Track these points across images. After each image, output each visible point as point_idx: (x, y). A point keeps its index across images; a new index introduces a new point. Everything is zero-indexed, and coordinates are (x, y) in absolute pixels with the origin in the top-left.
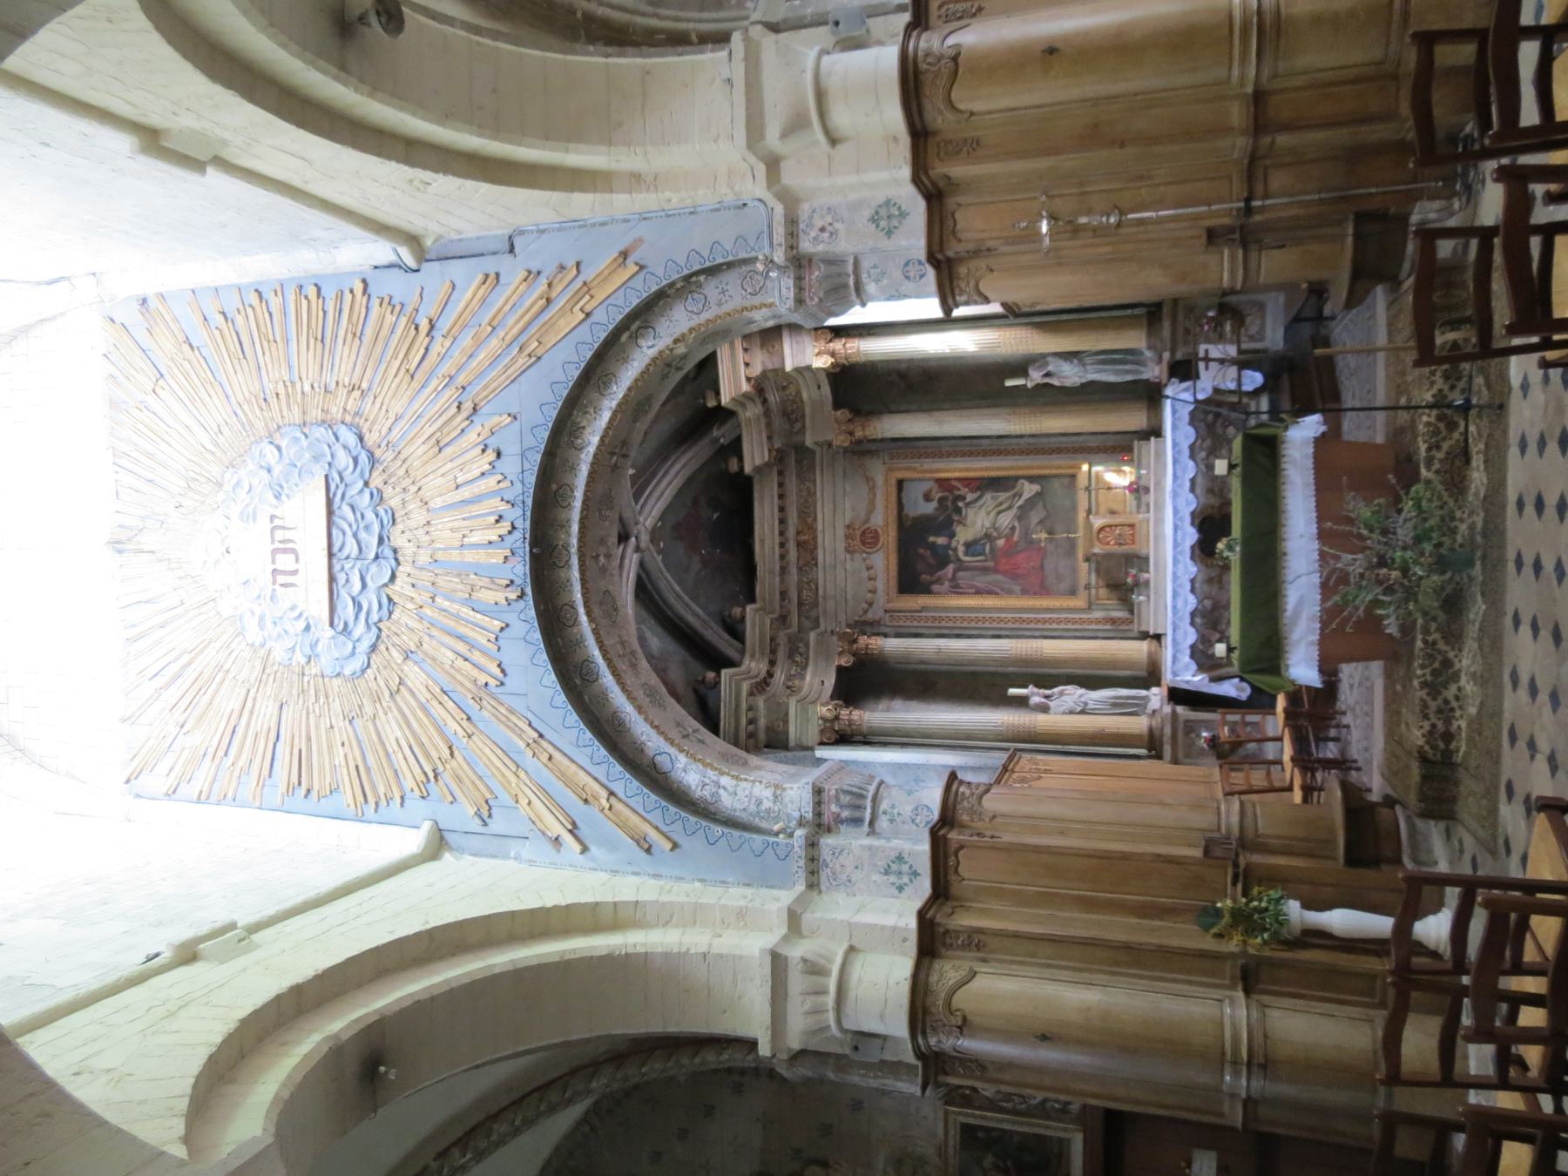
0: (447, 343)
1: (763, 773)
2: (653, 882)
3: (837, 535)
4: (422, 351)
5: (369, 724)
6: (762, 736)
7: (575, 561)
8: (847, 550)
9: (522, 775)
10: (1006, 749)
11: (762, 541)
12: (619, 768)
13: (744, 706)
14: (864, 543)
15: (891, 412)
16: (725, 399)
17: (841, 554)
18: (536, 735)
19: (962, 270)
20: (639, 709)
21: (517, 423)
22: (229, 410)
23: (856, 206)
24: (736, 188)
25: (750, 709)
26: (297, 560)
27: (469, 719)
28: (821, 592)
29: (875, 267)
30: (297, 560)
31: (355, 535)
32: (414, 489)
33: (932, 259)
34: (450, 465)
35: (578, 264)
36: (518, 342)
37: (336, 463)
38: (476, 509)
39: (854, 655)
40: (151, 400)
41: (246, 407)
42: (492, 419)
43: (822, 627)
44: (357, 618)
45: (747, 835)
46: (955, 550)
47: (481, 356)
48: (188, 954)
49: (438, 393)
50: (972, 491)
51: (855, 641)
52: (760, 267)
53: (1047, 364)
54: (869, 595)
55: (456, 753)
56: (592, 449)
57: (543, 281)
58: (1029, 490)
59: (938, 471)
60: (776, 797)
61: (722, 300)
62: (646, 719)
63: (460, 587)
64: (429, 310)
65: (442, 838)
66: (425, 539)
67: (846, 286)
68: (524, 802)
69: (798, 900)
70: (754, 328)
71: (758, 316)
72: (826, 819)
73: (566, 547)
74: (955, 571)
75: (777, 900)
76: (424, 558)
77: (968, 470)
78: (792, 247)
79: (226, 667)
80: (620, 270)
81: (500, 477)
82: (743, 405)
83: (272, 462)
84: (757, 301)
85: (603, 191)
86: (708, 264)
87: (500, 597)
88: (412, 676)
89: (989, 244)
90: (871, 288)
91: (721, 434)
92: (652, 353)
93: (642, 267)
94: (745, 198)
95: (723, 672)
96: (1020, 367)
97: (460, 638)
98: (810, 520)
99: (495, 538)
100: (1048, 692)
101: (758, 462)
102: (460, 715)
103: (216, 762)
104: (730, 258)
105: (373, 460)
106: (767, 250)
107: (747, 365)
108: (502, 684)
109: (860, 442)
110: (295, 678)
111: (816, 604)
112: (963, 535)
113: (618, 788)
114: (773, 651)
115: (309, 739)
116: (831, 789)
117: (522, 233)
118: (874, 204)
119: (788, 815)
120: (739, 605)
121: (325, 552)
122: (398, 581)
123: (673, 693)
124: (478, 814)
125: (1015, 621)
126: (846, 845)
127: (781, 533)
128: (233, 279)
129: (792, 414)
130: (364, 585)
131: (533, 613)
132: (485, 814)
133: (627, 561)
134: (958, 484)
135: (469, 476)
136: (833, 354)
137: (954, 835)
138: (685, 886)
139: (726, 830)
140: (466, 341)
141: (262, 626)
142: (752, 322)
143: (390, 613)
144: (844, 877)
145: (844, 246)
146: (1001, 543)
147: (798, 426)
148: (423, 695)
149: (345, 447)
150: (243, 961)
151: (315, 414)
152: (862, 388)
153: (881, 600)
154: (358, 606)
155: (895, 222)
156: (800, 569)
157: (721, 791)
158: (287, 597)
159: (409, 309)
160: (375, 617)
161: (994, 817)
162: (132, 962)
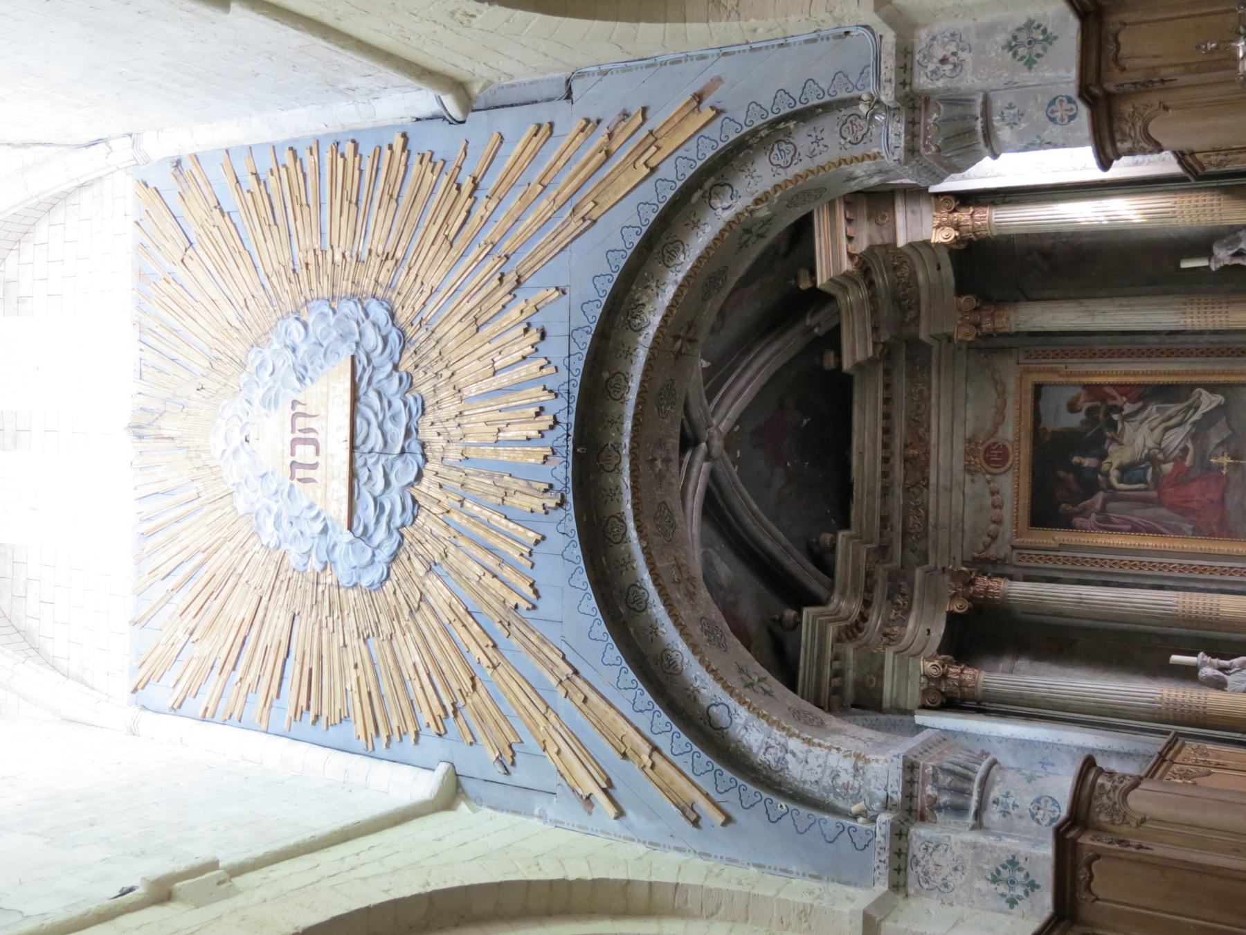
0: (492, 206)
1: (842, 738)
2: (698, 862)
3: (957, 452)
4: (464, 214)
5: (386, 644)
6: (850, 693)
7: (626, 465)
8: (967, 469)
9: (552, 718)
10: (1167, 733)
11: (861, 454)
12: (665, 718)
13: (829, 654)
14: (988, 461)
15: (1029, 299)
16: (822, 280)
17: (959, 475)
18: (570, 671)
19: (1127, 109)
20: (694, 648)
21: (566, 298)
22: (257, 282)
23: (988, 31)
24: (837, 13)
25: (836, 658)
26: (317, 453)
27: (495, 646)
28: (931, 520)
29: (1011, 107)
30: (317, 453)
31: (381, 426)
32: (446, 373)
33: (1085, 93)
34: (488, 347)
35: (644, 110)
36: (572, 204)
37: (364, 342)
38: (515, 399)
39: (970, 599)
40: (179, 271)
41: (274, 279)
42: (534, 294)
43: (932, 563)
44: (378, 521)
45: (817, 815)
46: (1107, 475)
47: (529, 221)
48: (162, 893)
49: (479, 263)
50: (1132, 401)
51: (972, 582)
52: (863, 109)
53: (1239, 240)
54: (993, 526)
55: (479, 686)
56: (651, 331)
57: (603, 130)
58: (1208, 401)
59: (1087, 374)
60: (856, 769)
61: (819, 148)
62: (701, 661)
63: (493, 490)
64: (473, 166)
65: (458, 785)
66: (456, 432)
67: (972, 131)
68: (552, 750)
69: (879, 903)
70: (854, 186)
71: (859, 170)
72: (919, 802)
73: (617, 447)
74: (1105, 501)
75: (851, 900)
76: (453, 455)
77: (1127, 374)
78: (904, 84)
79: (240, 570)
80: (693, 116)
81: (543, 362)
82: (844, 289)
83: (298, 341)
84: (858, 151)
85: (676, 20)
86: (799, 106)
87: (537, 503)
88: (433, 591)
89: (1164, 72)
90: (1004, 134)
91: (816, 323)
92: (728, 215)
93: (719, 112)
94: (848, 25)
95: (806, 611)
96: (1202, 244)
97: (489, 550)
98: (921, 431)
99: (534, 433)
100: (1226, 663)
101: (859, 357)
102: (484, 641)
103: (224, 675)
104: (827, 98)
105: (404, 340)
106: (872, 89)
107: (850, 239)
108: (534, 607)
109: (988, 336)
110: (309, 587)
111: (925, 534)
112: (1118, 456)
113: (663, 742)
114: (869, 589)
115: (320, 658)
116: (928, 765)
117: (581, 75)
118: (1010, 28)
119: (870, 794)
120: (828, 531)
121: (348, 444)
122: (425, 481)
123: (740, 631)
124: (499, 759)
125: (1183, 568)
126: (944, 839)
127: (885, 446)
128: (268, 136)
129: (904, 300)
130: (387, 484)
131: (572, 525)
132: (508, 761)
133: (695, 471)
134: (1114, 393)
135: (509, 360)
136: (957, 227)
137: (1086, 840)
138: (737, 871)
139: (792, 806)
140: (513, 202)
141: (277, 525)
142: (851, 178)
143: (415, 518)
144: (939, 880)
145: (970, 81)
146: (1168, 467)
147: (912, 314)
148: (446, 615)
149: (374, 324)
150: (222, 906)
151: (345, 286)
152: (997, 268)
153: (1007, 530)
154: (379, 507)
155: (1038, 49)
156: (906, 490)
157: (789, 757)
158: (305, 494)
159: (450, 167)
160: (397, 521)
161: (1143, 821)
162: (104, 894)
